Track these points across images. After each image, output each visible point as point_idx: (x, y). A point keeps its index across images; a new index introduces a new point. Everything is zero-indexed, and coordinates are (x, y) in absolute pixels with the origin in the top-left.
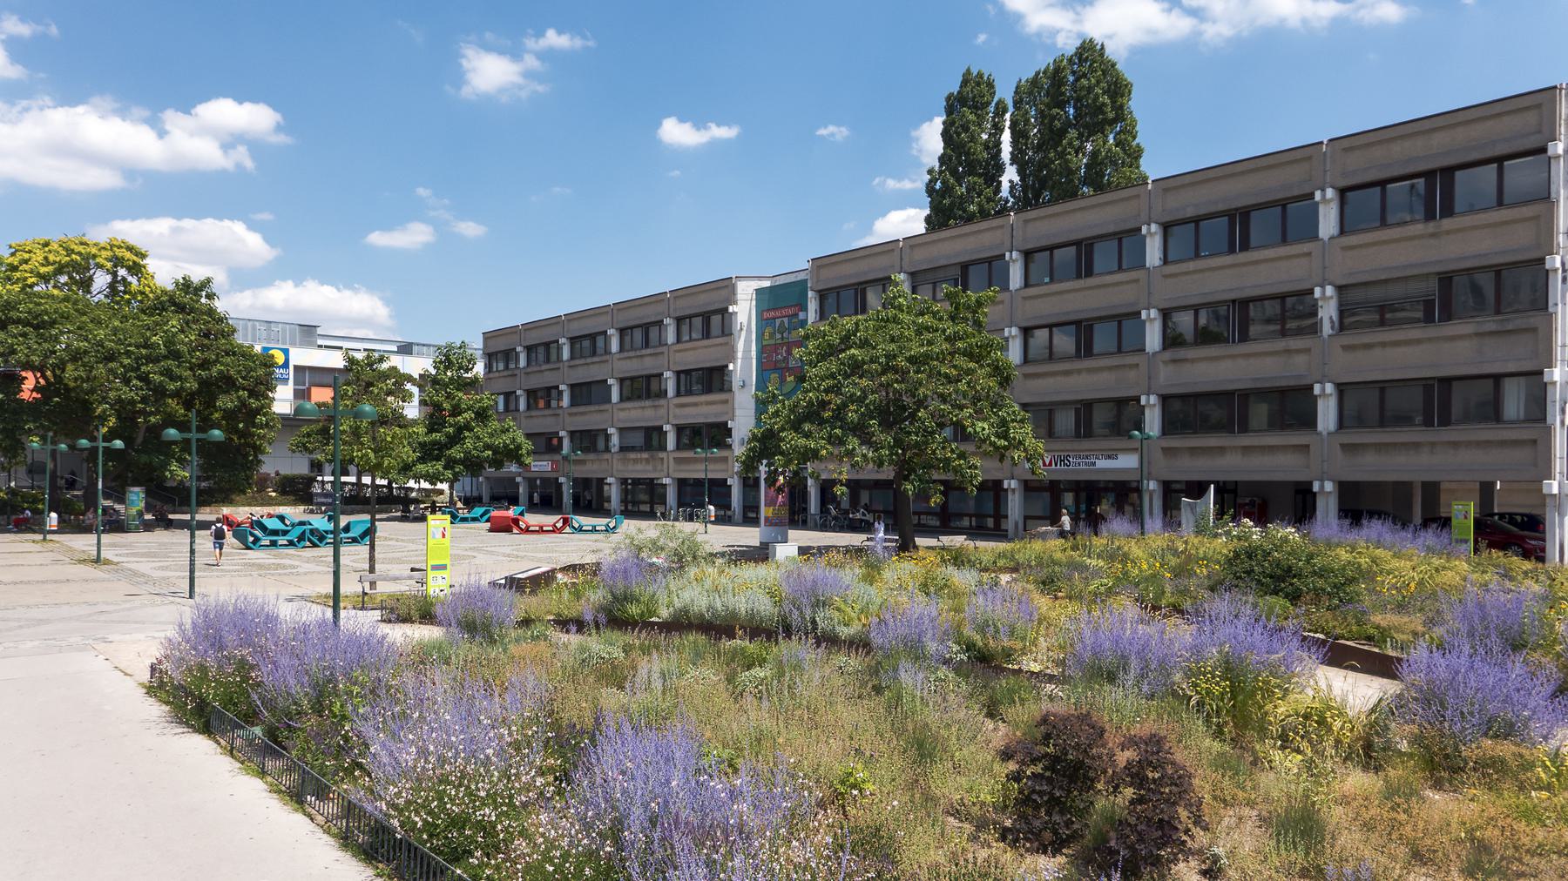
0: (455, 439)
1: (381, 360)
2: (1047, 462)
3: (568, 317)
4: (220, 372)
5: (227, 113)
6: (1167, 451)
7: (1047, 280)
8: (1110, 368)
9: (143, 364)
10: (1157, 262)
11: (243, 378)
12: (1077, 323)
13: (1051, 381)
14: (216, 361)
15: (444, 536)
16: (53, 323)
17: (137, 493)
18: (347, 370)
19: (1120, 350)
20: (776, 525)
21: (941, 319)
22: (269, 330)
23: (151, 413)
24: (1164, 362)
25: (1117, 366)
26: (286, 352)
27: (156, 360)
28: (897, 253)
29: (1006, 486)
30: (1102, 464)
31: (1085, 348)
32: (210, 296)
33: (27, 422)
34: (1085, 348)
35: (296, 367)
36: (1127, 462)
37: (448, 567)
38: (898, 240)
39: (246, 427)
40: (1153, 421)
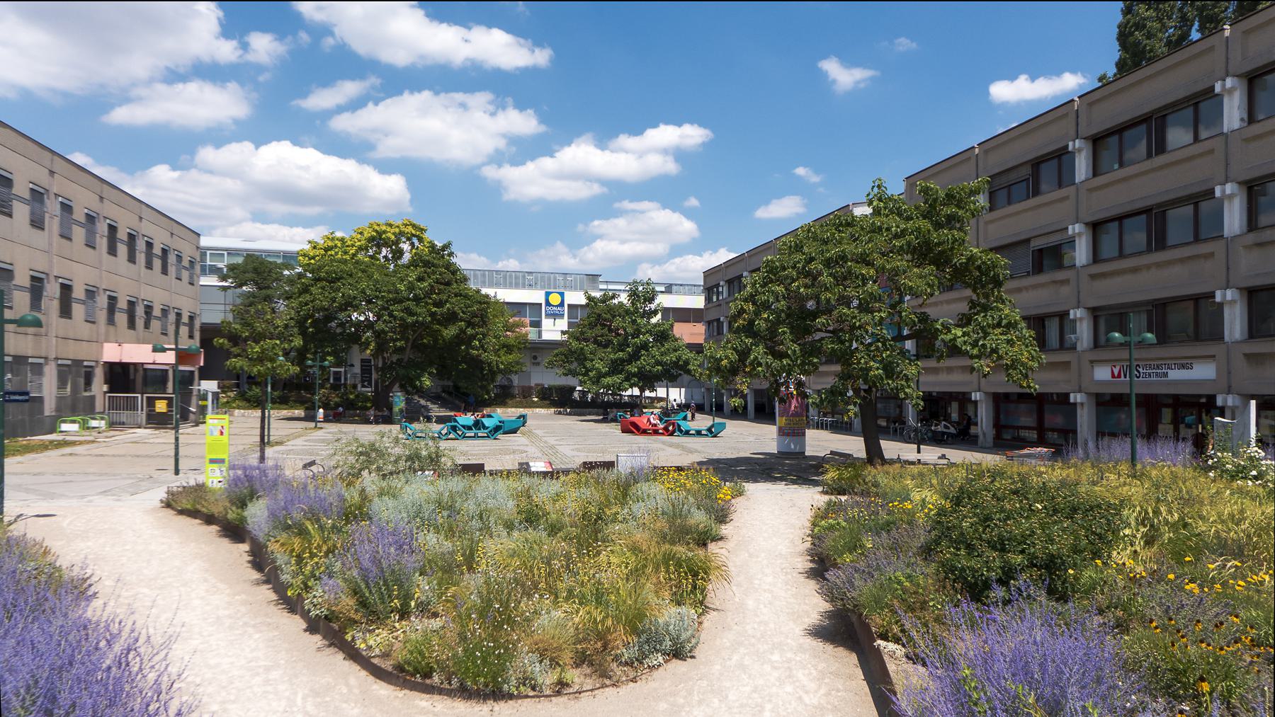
0: (635, 357)
1: (613, 297)
2: (1116, 374)
3: (749, 254)
4: (448, 309)
5: (666, 135)
6: (1250, 357)
7: (1116, 166)
8: (1182, 261)
9: (391, 305)
10: (1236, 124)
11: (463, 312)
12: (1147, 211)
13: (1118, 280)
14: (447, 301)
15: (222, 433)
16: (338, 279)
17: (399, 397)
18: (587, 305)
19: (1197, 239)
20: (788, 435)
21: (909, 218)
22: (565, 279)
23: (397, 340)
24: (1246, 247)
25: (1189, 258)
26: (562, 294)
27: (400, 302)
28: (973, 161)
29: (1072, 400)
30: (1175, 374)
31: (1158, 240)
32: (451, 254)
33: (327, 347)
34: (1158, 240)
35: (569, 305)
36: (1203, 372)
37: (207, 461)
38: (973, 147)
39: (467, 348)
40: (1235, 323)
